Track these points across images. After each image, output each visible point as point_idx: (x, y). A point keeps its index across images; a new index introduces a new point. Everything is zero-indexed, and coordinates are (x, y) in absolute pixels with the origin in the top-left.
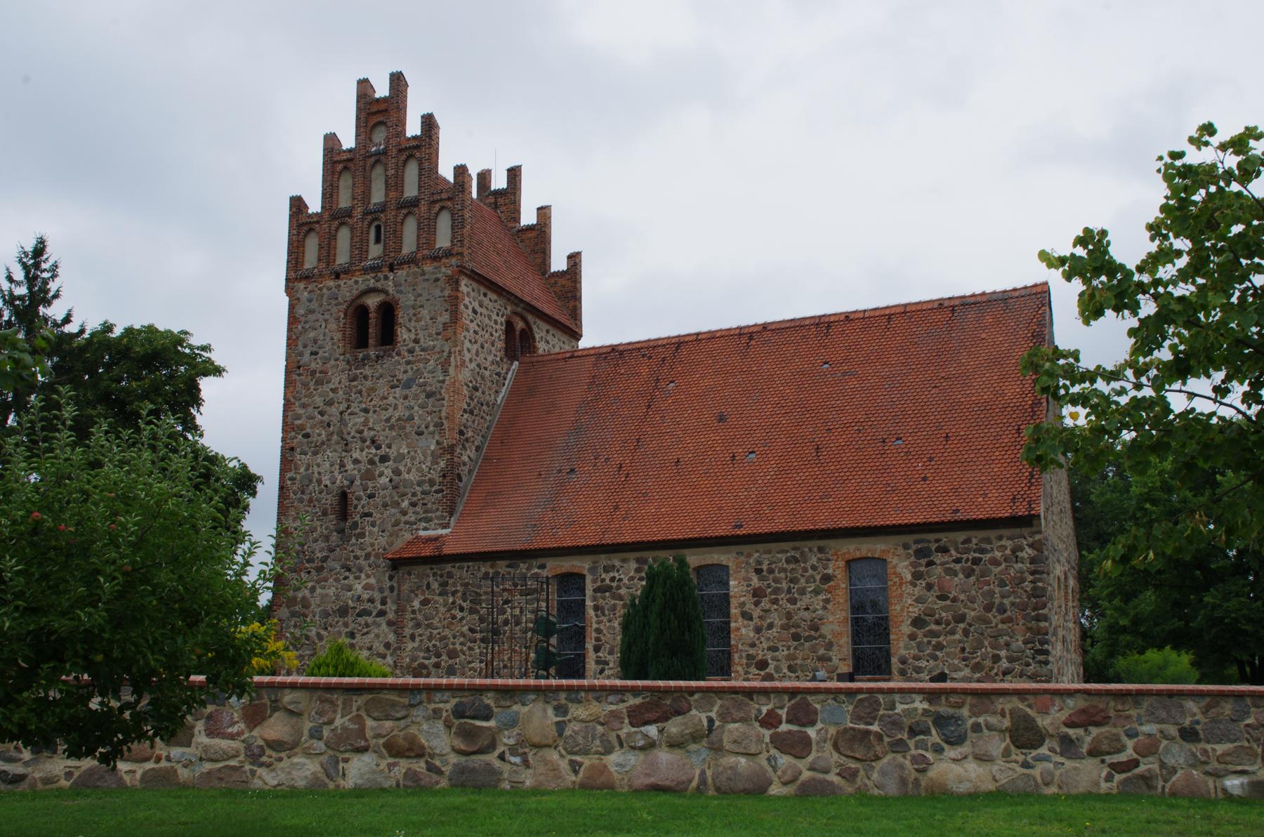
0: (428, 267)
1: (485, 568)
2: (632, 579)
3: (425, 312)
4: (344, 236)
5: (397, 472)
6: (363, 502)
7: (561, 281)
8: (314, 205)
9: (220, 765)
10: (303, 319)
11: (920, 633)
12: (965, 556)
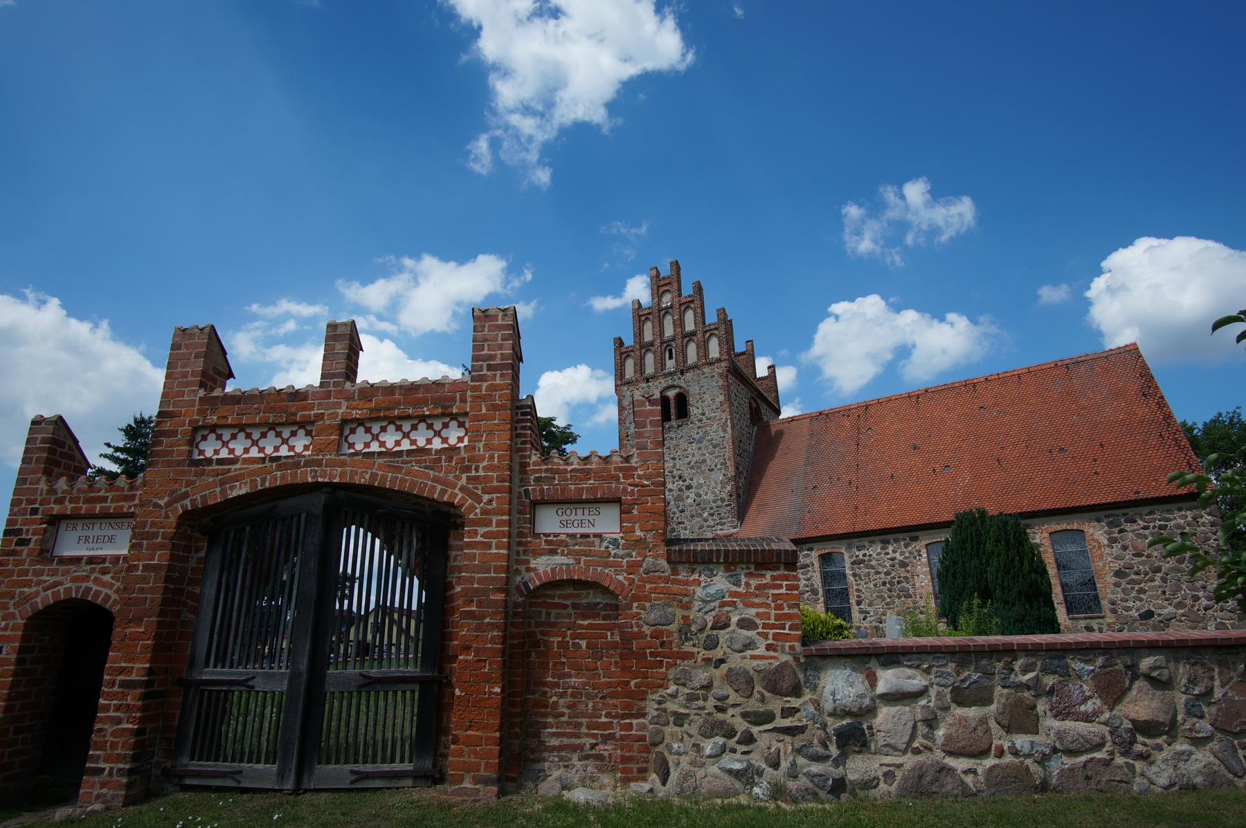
0: (706, 370)
2: (879, 554)
3: (706, 396)
4: (650, 359)
5: (698, 495)
7: (766, 382)
8: (629, 341)
9: (1083, 758)
11: (1123, 582)
12: (1152, 525)
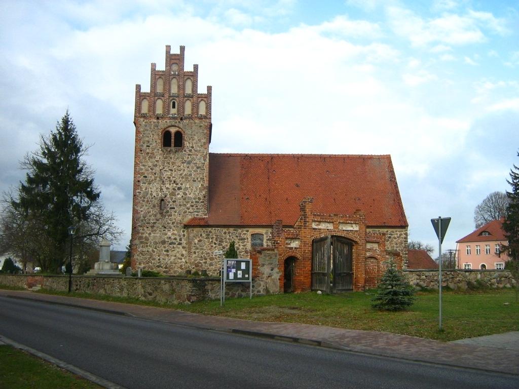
1: (225, 230)
3: (196, 137)
6: (171, 203)
10: (143, 133)
